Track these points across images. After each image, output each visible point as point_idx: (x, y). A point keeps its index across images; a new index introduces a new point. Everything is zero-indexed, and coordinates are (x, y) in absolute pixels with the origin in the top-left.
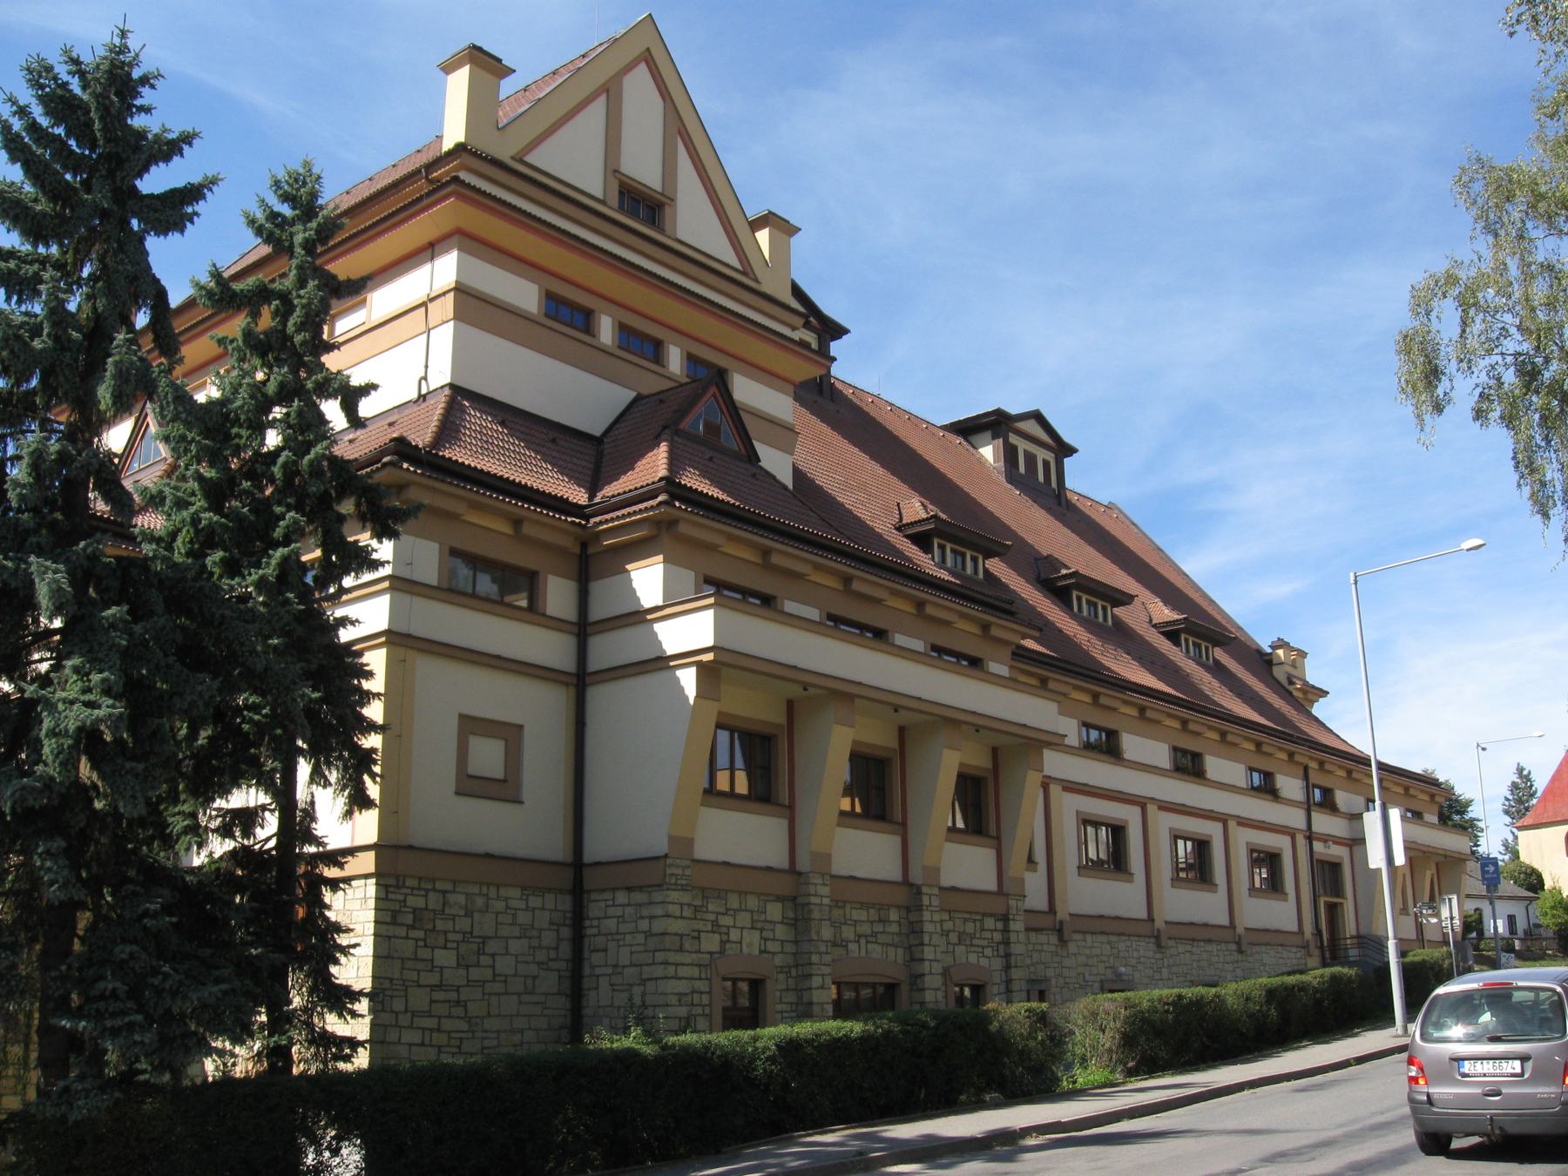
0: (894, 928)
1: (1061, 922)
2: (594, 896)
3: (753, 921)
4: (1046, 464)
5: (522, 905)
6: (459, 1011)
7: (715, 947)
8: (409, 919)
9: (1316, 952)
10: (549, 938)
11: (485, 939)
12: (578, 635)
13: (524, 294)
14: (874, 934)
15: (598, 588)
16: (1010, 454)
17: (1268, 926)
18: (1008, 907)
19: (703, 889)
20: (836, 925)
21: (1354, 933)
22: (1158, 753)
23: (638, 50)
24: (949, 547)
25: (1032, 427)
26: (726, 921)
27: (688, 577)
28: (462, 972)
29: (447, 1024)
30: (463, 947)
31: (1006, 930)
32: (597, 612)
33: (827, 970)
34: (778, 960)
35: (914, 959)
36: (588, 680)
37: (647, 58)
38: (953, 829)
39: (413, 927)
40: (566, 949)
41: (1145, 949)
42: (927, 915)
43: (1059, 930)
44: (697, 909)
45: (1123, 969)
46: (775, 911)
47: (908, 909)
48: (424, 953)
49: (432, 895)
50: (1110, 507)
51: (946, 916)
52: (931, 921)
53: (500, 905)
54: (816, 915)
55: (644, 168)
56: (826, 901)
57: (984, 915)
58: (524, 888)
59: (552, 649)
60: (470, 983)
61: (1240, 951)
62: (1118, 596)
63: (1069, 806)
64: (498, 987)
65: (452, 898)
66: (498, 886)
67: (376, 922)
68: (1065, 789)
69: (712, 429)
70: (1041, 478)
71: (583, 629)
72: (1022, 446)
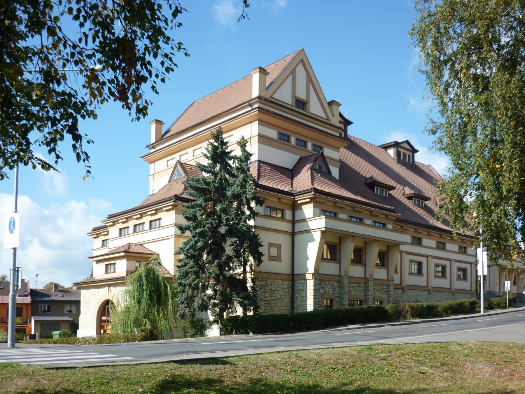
0: (362, 288)
1: (403, 287)
2: (296, 281)
3: (331, 287)
4: (409, 156)
5: (281, 283)
6: (269, 306)
7: (323, 292)
8: (260, 287)
9: (476, 295)
10: (287, 290)
11: (274, 291)
12: (292, 223)
13: (273, 134)
14: (358, 289)
15: (297, 213)
16: (398, 154)
17: (439, 286)
18: (389, 283)
19: (321, 280)
20: (349, 287)
21: (488, 290)
22: (433, 243)
23: (299, 60)
24: (379, 188)
25: (406, 145)
26: (325, 286)
27: (318, 210)
28: (270, 298)
29: (267, 308)
30: (270, 292)
31: (389, 289)
32: (297, 218)
33: (347, 297)
34: (336, 295)
35: (366, 295)
36: (295, 234)
37: (302, 61)
38: (377, 264)
39: (260, 288)
40: (290, 293)
41: (425, 294)
42: (370, 285)
43: (403, 289)
44: (319, 284)
45: (419, 299)
46: (336, 284)
47: (365, 284)
48: (263, 294)
49: (264, 282)
50: (428, 166)
51: (374, 285)
52: (371, 287)
53: (277, 284)
54: (345, 285)
55: (301, 95)
56: (347, 282)
57: (383, 285)
58: (282, 280)
59: (286, 227)
60: (272, 300)
61: (452, 295)
62: (426, 198)
63: (407, 258)
64: (277, 301)
65: (268, 282)
66: (277, 279)
67: (314, 286)
68: (406, 254)
69: (320, 167)
70: (407, 160)
71: (293, 222)
72: (402, 151)
